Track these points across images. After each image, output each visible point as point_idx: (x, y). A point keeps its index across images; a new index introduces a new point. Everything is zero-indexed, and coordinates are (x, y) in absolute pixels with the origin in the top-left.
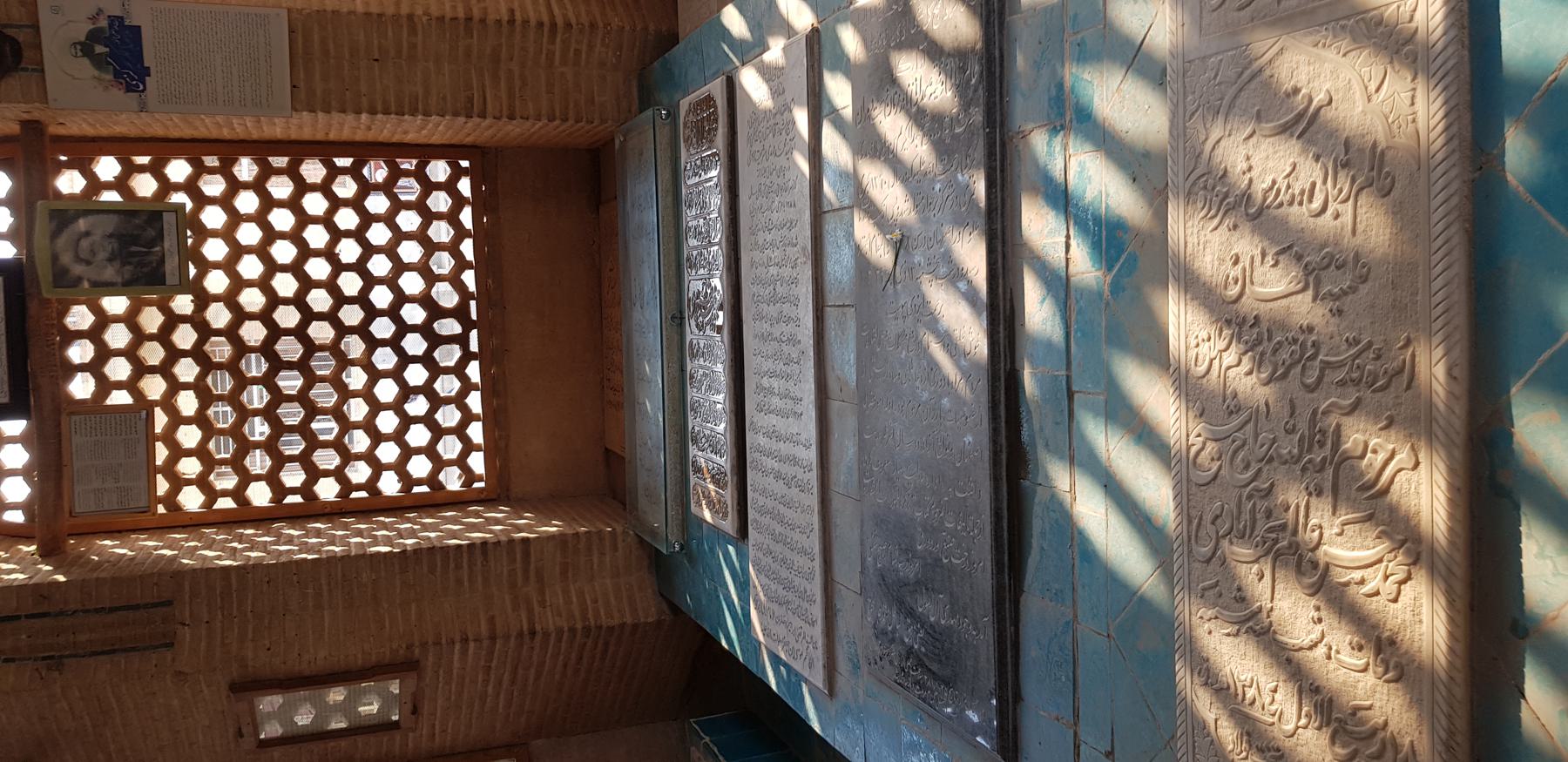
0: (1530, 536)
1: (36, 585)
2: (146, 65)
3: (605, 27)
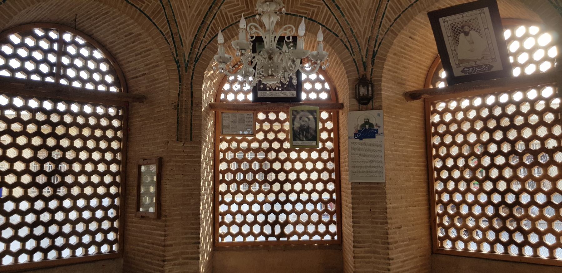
1: (201, 103)
2: (363, 139)
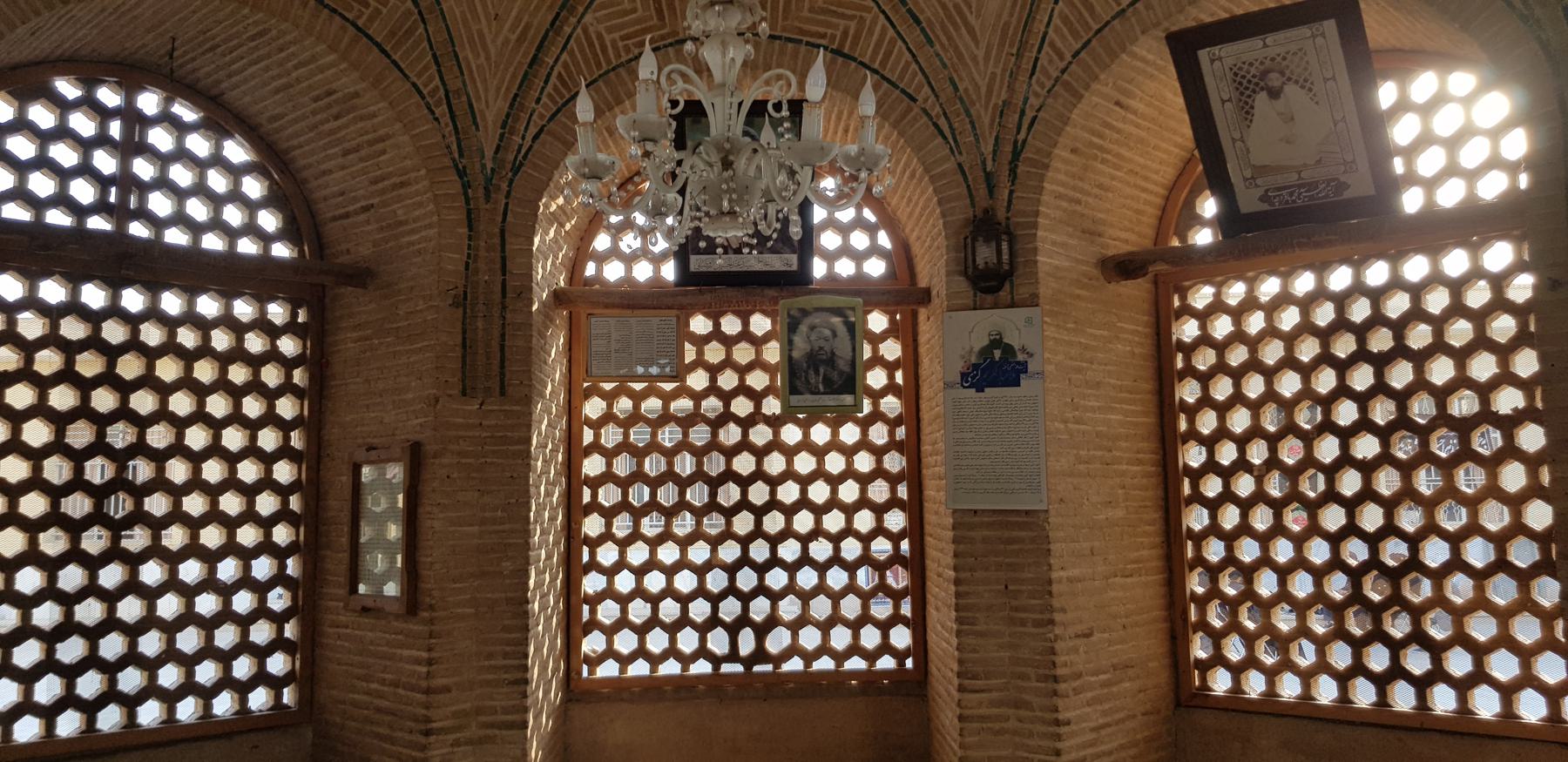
1: (531, 289)
2: (987, 390)
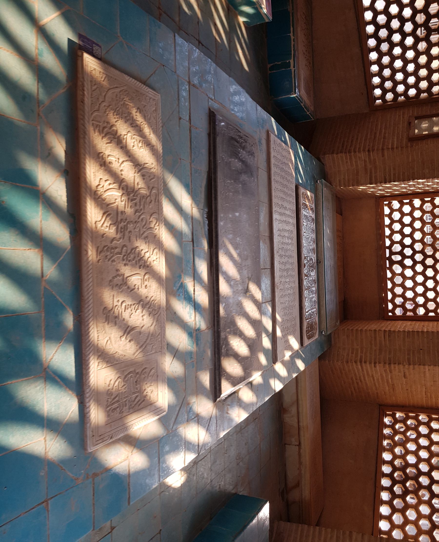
0: (64, 202)
3: (343, 362)
